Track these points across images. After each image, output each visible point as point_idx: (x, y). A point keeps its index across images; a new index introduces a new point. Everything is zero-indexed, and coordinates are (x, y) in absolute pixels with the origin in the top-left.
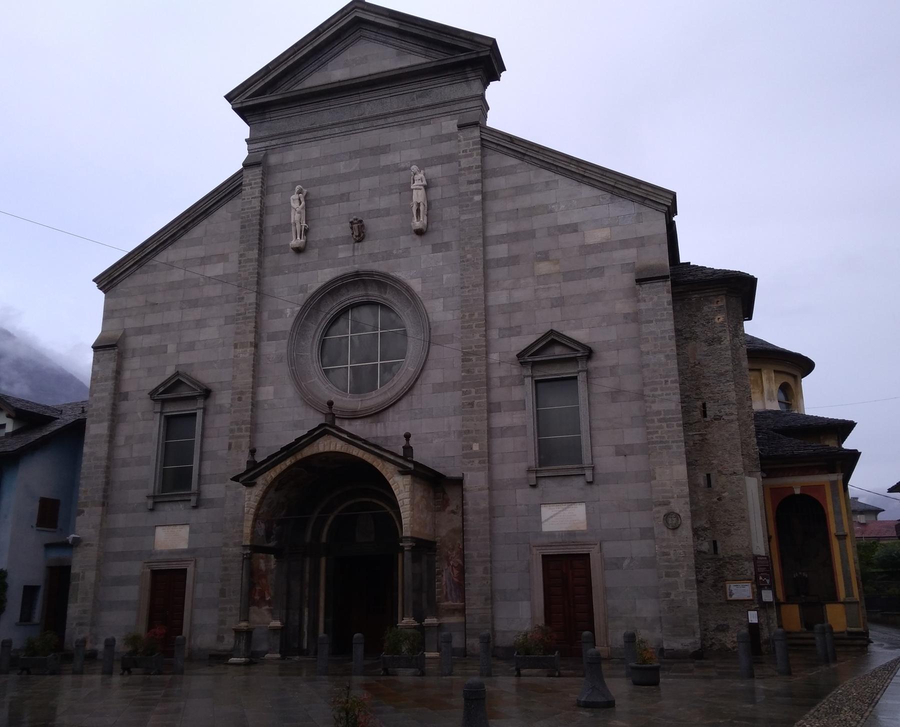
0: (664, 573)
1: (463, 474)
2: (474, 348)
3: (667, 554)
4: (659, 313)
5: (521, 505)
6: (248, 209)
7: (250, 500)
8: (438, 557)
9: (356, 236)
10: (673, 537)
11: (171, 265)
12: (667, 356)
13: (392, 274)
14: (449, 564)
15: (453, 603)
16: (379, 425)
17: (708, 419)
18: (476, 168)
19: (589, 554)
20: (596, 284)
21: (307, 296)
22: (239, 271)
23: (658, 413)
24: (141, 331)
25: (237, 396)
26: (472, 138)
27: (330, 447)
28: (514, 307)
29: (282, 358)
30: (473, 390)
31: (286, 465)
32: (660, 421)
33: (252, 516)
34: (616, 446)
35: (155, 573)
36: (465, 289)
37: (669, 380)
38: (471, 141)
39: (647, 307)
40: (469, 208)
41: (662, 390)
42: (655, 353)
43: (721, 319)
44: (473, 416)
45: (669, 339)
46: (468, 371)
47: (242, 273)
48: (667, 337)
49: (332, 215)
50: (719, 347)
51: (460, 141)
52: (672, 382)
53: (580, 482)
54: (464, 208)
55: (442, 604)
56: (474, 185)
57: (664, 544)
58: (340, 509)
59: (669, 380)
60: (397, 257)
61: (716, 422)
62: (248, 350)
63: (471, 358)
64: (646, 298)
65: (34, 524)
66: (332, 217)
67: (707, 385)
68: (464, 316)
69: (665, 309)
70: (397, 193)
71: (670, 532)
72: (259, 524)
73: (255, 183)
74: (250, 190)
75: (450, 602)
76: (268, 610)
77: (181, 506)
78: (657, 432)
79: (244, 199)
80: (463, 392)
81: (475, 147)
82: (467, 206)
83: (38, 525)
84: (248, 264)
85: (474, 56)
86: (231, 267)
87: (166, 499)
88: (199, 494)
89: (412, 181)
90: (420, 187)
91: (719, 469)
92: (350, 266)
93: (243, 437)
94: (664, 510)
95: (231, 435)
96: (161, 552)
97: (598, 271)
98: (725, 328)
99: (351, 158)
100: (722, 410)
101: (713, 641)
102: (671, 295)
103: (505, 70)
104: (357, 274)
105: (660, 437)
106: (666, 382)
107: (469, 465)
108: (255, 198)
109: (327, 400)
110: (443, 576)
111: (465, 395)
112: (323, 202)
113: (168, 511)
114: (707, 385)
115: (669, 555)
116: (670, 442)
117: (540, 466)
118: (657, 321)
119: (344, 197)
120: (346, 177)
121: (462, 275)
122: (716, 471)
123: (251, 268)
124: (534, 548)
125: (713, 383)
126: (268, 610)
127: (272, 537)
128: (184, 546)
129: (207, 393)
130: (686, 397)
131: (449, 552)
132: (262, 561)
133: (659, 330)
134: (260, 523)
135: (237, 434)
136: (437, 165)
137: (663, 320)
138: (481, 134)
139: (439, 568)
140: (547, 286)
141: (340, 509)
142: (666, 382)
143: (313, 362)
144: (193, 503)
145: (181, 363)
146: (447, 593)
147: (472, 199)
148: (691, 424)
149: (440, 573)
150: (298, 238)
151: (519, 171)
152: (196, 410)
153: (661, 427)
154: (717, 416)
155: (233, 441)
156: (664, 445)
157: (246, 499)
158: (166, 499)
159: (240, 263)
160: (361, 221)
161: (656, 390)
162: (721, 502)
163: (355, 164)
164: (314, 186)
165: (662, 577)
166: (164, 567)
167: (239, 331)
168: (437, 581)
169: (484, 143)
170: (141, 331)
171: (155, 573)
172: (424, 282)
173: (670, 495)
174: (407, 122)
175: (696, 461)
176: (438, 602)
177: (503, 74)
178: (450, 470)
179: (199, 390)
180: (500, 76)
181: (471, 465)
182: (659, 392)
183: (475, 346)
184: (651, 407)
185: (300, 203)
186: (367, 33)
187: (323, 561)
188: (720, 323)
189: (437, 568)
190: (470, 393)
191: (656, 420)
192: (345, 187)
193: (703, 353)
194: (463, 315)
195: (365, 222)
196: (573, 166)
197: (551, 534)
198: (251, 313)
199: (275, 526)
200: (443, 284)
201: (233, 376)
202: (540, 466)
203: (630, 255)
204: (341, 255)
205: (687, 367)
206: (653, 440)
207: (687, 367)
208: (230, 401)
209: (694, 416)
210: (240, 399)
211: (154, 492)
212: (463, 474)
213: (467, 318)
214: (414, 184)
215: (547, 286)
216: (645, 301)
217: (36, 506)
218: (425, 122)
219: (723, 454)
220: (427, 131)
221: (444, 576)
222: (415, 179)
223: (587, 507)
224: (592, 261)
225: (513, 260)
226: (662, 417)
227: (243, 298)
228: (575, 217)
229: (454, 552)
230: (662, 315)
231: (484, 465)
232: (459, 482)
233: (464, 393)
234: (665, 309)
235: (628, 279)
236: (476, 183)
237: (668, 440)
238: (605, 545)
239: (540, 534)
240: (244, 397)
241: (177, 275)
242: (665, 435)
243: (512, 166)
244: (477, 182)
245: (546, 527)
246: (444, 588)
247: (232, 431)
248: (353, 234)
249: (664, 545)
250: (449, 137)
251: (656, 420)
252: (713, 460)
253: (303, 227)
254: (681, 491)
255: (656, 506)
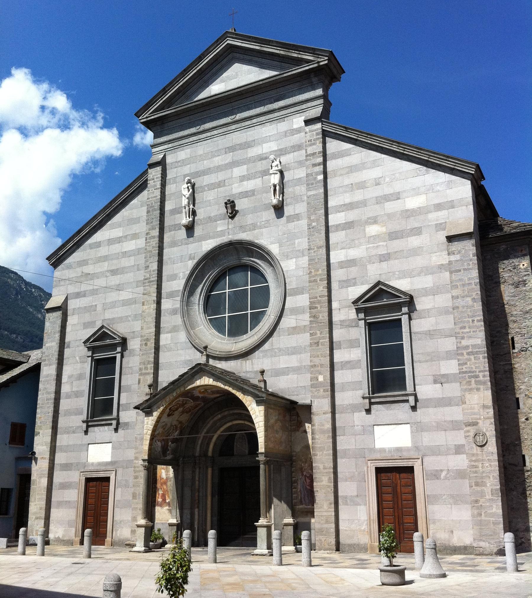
0: (474, 484)
1: (311, 400)
2: (319, 298)
3: (476, 467)
4: (465, 264)
5: (357, 426)
6: (152, 198)
7: (147, 424)
8: (294, 468)
9: (230, 214)
10: (481, 453)
11: (98, 245)
12: (474, 300)
13: (256, 241)
14: (302, 475)
15: (306, 507)
16: (248, 362)
17: (516, 351)
18: (318, 154)
19: (413, 467)
20: (414, 241)
21: (195, 261)
22: (146, 246)
23: (467, 347)
24: (78, 295)
25: (144, 342)
26: (315, 130)
27: (205, 381)
28: (350, 263)
29: (176, 311)
30: (318, 332)
31: (173, 396)
32: (468, 354)
33: (149, 436)
34: (433, 375)
35: (88, 480)
36: (311, 251)
37: (476, 319)
38: (314, 133)
39: (456, 259)
40: (314, 185)
41: (469, 328)
42: (463, 297)
43: (526, 265)
44: (319, 353)
45: (475, 285)
46: (314, 317)
47: (148, 247)
48: (473, 283)
49: (213, 198)
50: (524, 288)
51: (306, 133)
52: (478, 321)
53: (406, 406)
54: (310, 186)
55: (297, 507)
56: (317, 167)
57: (474, 459)
58: (222, 429)
59: (476, 319)
60: (260, 227)
61: (523, 353)
62: (152, 306)
63: (316, 306)
64: (455, 252)
65: (8, 441)
66: (213, 199)
67: (515, 322)
68: (311, 272)
69: (471, 260)
70: (259, 177)
71: (479, 448)
72: (156, 442)
73: (157, 178)
74: (153, 183)
75: (304, 505)
76: (168, 510)
77: (106, 428)
78: (466, 364)
79: (149, 191)
80: (311, 334)
81: (318, 137)
82: (312, 184)
83: (10, 443)
84: (152, 240)
85: (316, 65)
86: (141, 243)
87: (96, 423)
88: (118, 419)
89: (271, 168)
90: (276, 172)
91: (526, 393)
92: (225, 237)
93: (148, 374)
94: (472, 431)
95: (140, 372)
96: (92, 464)
97: (417, 231)
98: (528, 273)
99: (226, 153)
100: (528, 343)
101: (523, 540)
102: (475, 248)
103: (344, 72)
104: (231, 244)
105: (469, 368)
106: (473, 321)
107: (316, 394)
108: (157, 189)
109: (204, 345)
110: (298, 484)
111: (312, 336)
112: (206, 189)
113: (97, 432)
114: (515, 322)
115: (478, 467)
116: (477, 372)
117: (373, 394)
118: (464, 269)
119: (220, 184)
120: (219, 169)
121: (309, 239)
122: (523, 395)
123: (154, 243)
124: (369, 462)
125: (520, 320)
126: (168, 510)
127: (168, 452)
128: (108, 459)
129: (124, 342)
130: (497, 333)
131: (302, 465)
132: (163, 471)
133: (466, 278)
134: (157, 441)
135: (144, 371)
136: (290, 153)
137: (470, 269)
138: (322, 126)
139: (295, 478)
140: (376, 245)
141: (222, 429)
142: (473, 321)
143: (200, 313)
144: (114, 426)
145: (106, 318)
146: (301, 498)
147: (316, 178)
148: (502, 356)
149: (296, 482)
150: (188, 218)
151: (353, 153)
152: (116, 354)
153: (470, 360)
154: (524, 348)
155: (141, 377)
156: (473, 374)
157: (145, 423)
158: (96, 423)
159: (146, 240)
160: (233, 202)
161: (464, 327)
162: (528, 421)
163: (229, 158)
164: (200, 176)
165: (472, 487)
166: (94, 475)
167: (145, 292)
168: (294, 489)
169: (325, 133)
170: (78, 295)
171: (88, 480)
172: (280, 246)
173: (478, 417)
174: (267, 121)
175: (507, 387)
176: (295, 505)
177: (343, 76)
178: (302, 399)
179: (117, 338)
180: (341, 77)
181: (318, 393)
182: (467, 330)
183: (320, 296)
184: (461, 342)
185: (189, 190)
186: (238, 55)
187: (210, 471)
188: (524, 269)
189: (294, 478)
190: (316, 334)
191: (465, 354)
192: (221, 176)
193: (511, 295)
194: (310, 272)
195: (236, 202)
196: (395, 146)
197: (382, 450)
198: (154, 278)
199: (170, 443)
200: (295, 247)
201: (142, 327)
202: (373, 394)
203: (441, 216)
204: (219, 229)
205: (497, 307)
206: (463, 370)
207: (497, 307)
208: (139, 346)
209: (504, 348)
210: (146, 345)
211: (87, 418)
212: (311, 400)
213: (313, 274)
214: (272, 170)
215: (376, 245)
216: (454, 254)
217: (9, 428)
218: (282, 118)
219: (529, 380)
220: (283, 126)
221: (299, 484)
222: (273, 166)
223: (411, 427)
224: (413, 223)
225: (348, 225)
226: (470, 350)
227: (148, 266)
228: (397, 187)
229: (307, 465)
230: (469, 264)
231: (327, 393)
232: (308, 407)
233: (311, 334)
234: (471, 260)
235: (442, 237)
236: (319, 165)
237: (475, 370)
238: (426, 459)
239: (373, 450)
240: (149, 343)
241: (103, 251)
242: (473, 366)
243: (347, 149)
244: (319, 164)
245: (379, 444)
246: (299, 494)
247: (141, 369)
248: (227, 212)
249: (473, 459)
250: (299, 131)
251: (465, 354)
252: (521, 386)
253: (191, 209)
254: (487, 413)
255: (466, 426)
